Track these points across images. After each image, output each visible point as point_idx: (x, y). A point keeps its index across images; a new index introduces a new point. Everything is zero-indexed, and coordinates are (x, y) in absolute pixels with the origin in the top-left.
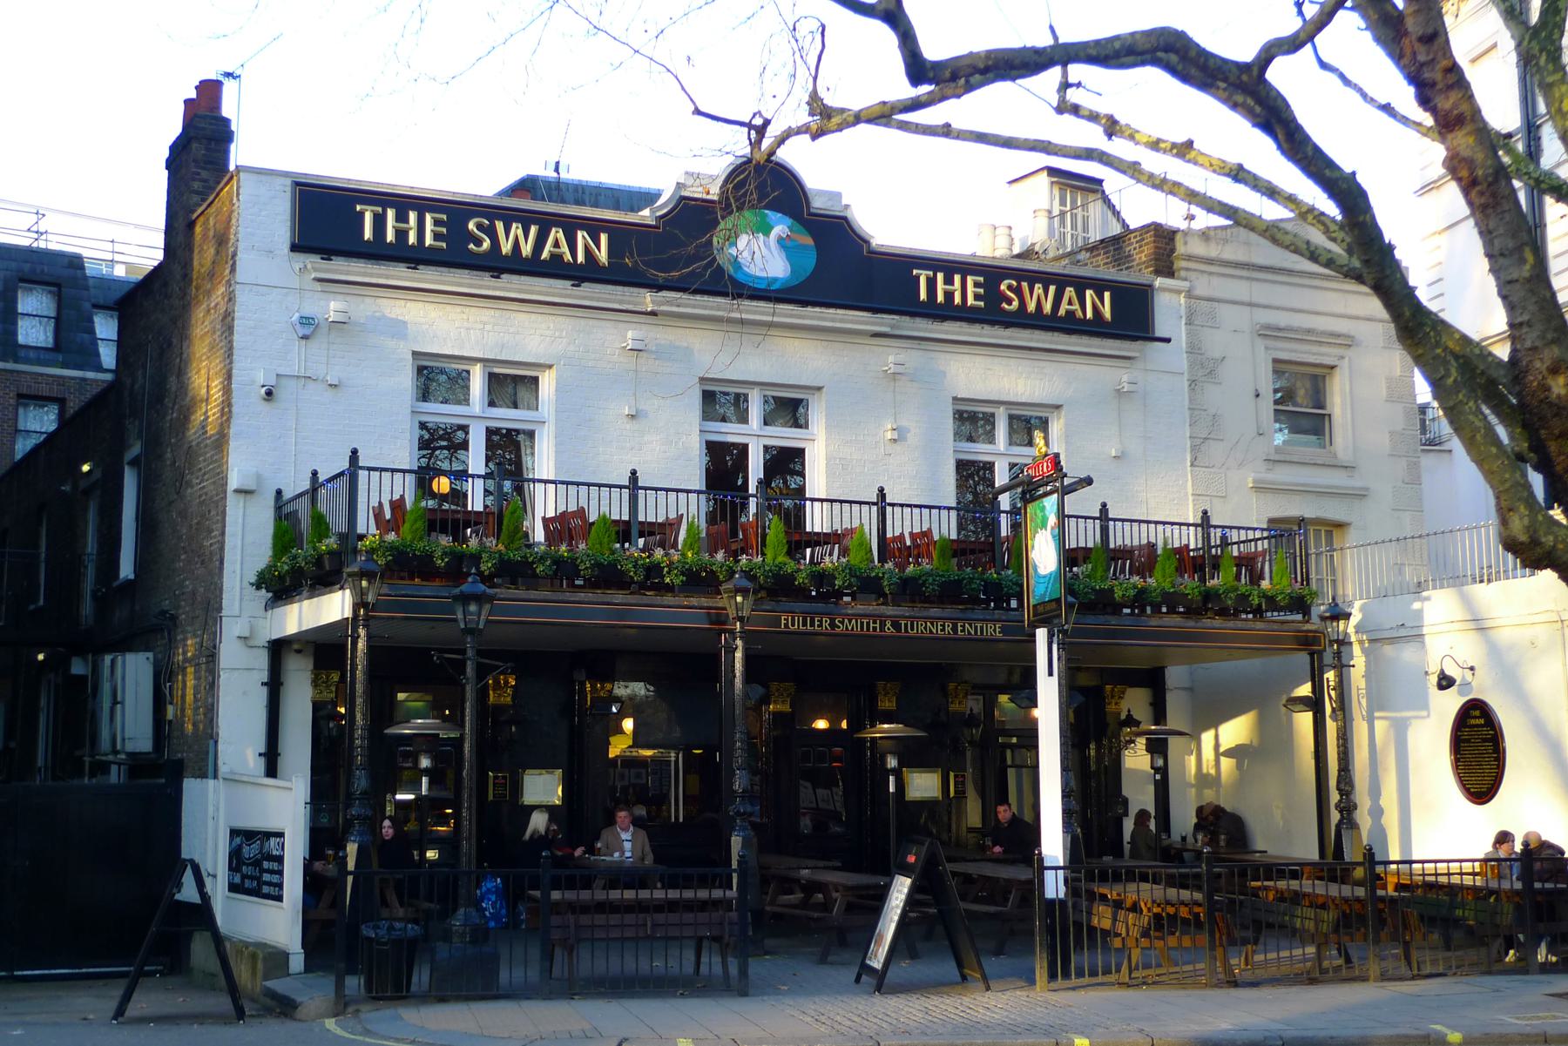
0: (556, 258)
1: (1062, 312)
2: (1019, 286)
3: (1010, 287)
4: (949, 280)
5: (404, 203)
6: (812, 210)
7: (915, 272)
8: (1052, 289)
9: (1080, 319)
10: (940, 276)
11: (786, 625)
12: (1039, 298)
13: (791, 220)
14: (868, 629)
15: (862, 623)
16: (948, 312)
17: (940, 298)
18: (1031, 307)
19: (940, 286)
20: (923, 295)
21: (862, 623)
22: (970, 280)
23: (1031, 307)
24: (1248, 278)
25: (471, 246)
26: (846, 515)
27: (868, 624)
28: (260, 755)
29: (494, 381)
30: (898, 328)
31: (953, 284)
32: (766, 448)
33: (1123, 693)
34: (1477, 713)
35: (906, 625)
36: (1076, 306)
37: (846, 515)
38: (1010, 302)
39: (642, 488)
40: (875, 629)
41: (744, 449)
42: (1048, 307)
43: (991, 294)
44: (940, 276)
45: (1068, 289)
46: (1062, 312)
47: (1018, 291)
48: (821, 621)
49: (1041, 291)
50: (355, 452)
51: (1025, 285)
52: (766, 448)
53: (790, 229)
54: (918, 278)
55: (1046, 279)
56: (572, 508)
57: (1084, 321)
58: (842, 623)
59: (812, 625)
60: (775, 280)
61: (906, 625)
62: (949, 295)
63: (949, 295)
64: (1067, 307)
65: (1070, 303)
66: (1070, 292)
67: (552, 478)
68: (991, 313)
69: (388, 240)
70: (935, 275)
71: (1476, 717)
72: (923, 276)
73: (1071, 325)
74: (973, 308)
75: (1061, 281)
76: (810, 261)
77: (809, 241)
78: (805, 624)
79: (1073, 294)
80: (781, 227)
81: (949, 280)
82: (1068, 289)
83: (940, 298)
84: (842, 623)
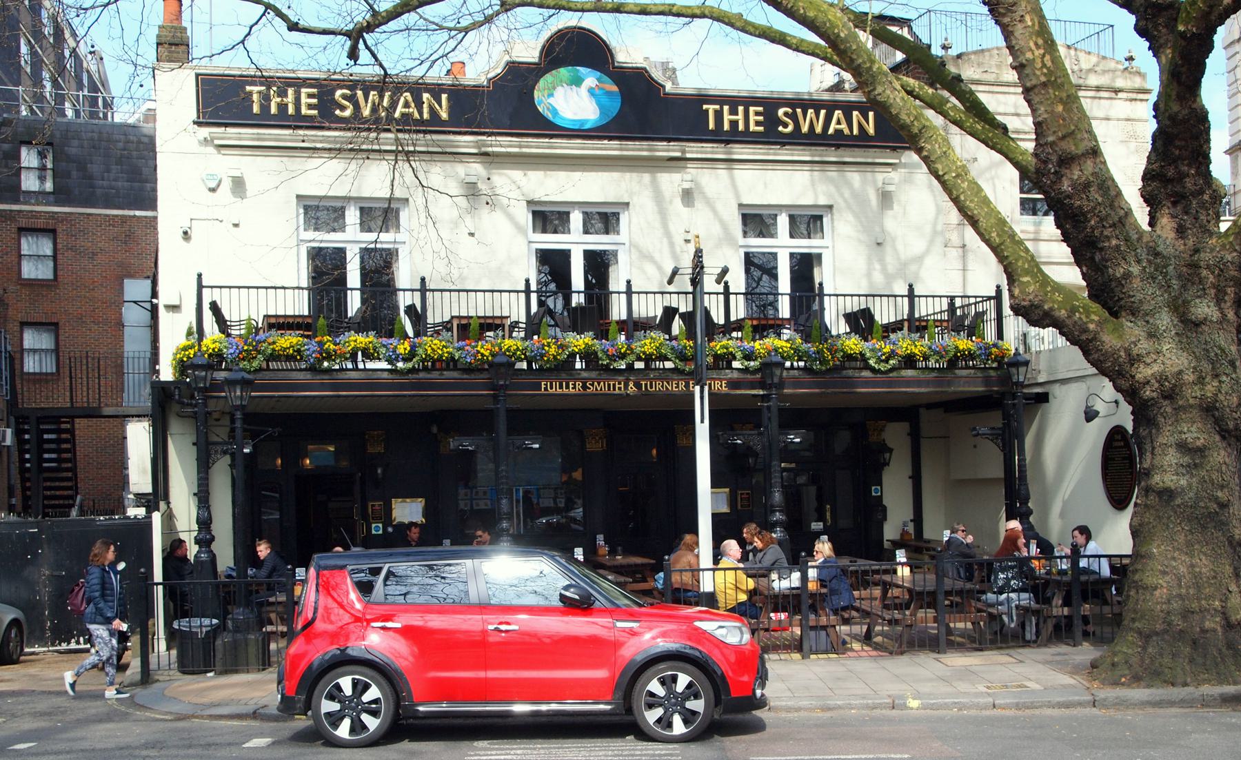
0: (839, 132)
1: (831, 131)
2: (795, 113)
3: (786, 114)
4: (734, 112)
5: (734, 102)
6: (616, 64)
7: (705, 107)
8: (823, 112)
9: (847, 136)
10: (726, 108)
11: (546, 389)
12: (810, 121)
13: (599, 73)
14: (614, 389)
15: (609, 385)
16: (735, 136)
17: (726, 127)
18: (805, 129)
19: (727, 117)
20: (711, 126)
21: (609, 385)
22: (752, 109)
23: (805, 129)
24: (989, 92)
25: (781, 128)
26: (464, 304)
27: (614, 385)
28: (195, 494)
29: (587, 217)
30: (731, 153)
31: (737, 114)
32: (792, 255)
33: (884, 426)
34: (1119, 437)
35: (646, 385)
36: (844, 126)
37: (464, 304)
38: (786, 125)
39: (430, 290)
40: (620, 388)
41: (342, 252)
42: (819, 129)
43: (771, 121)
44: (726, 108)
45: (837, 112)
46: (831, 131)
47: (793, 117)
48: (574, 385)
49: (813, 115)
50: (200, 276)
51: (799, 111)
52: (792, 255)
53: (598, 80)
54: (707, 111)
55: (817, 105)
56: (863, 307)
57: (852, 137)
58: (593, 385)
59: (567, 387)
60: (587, 121)
61: (646, 385)
62: (734, 124)
63: (734, 124)
64: (404, 110)
65: (839, 123)
66: (838, 113)
67: (408, 287)
68: (770, 135)
69: (272, 113)
70: (722, 108)
71: (1118, 440)
72: (711, 108)
73: (839, 141)
74: (755, 133)
75: (831, 107)
76: (615, 105)
77: (615, 88)
78: (561, 387)
79: (841, 116)
80: (591, 79)
81: (734, 112)
82: (372, 93)
83: (726, 127)
84: (593, 385)
